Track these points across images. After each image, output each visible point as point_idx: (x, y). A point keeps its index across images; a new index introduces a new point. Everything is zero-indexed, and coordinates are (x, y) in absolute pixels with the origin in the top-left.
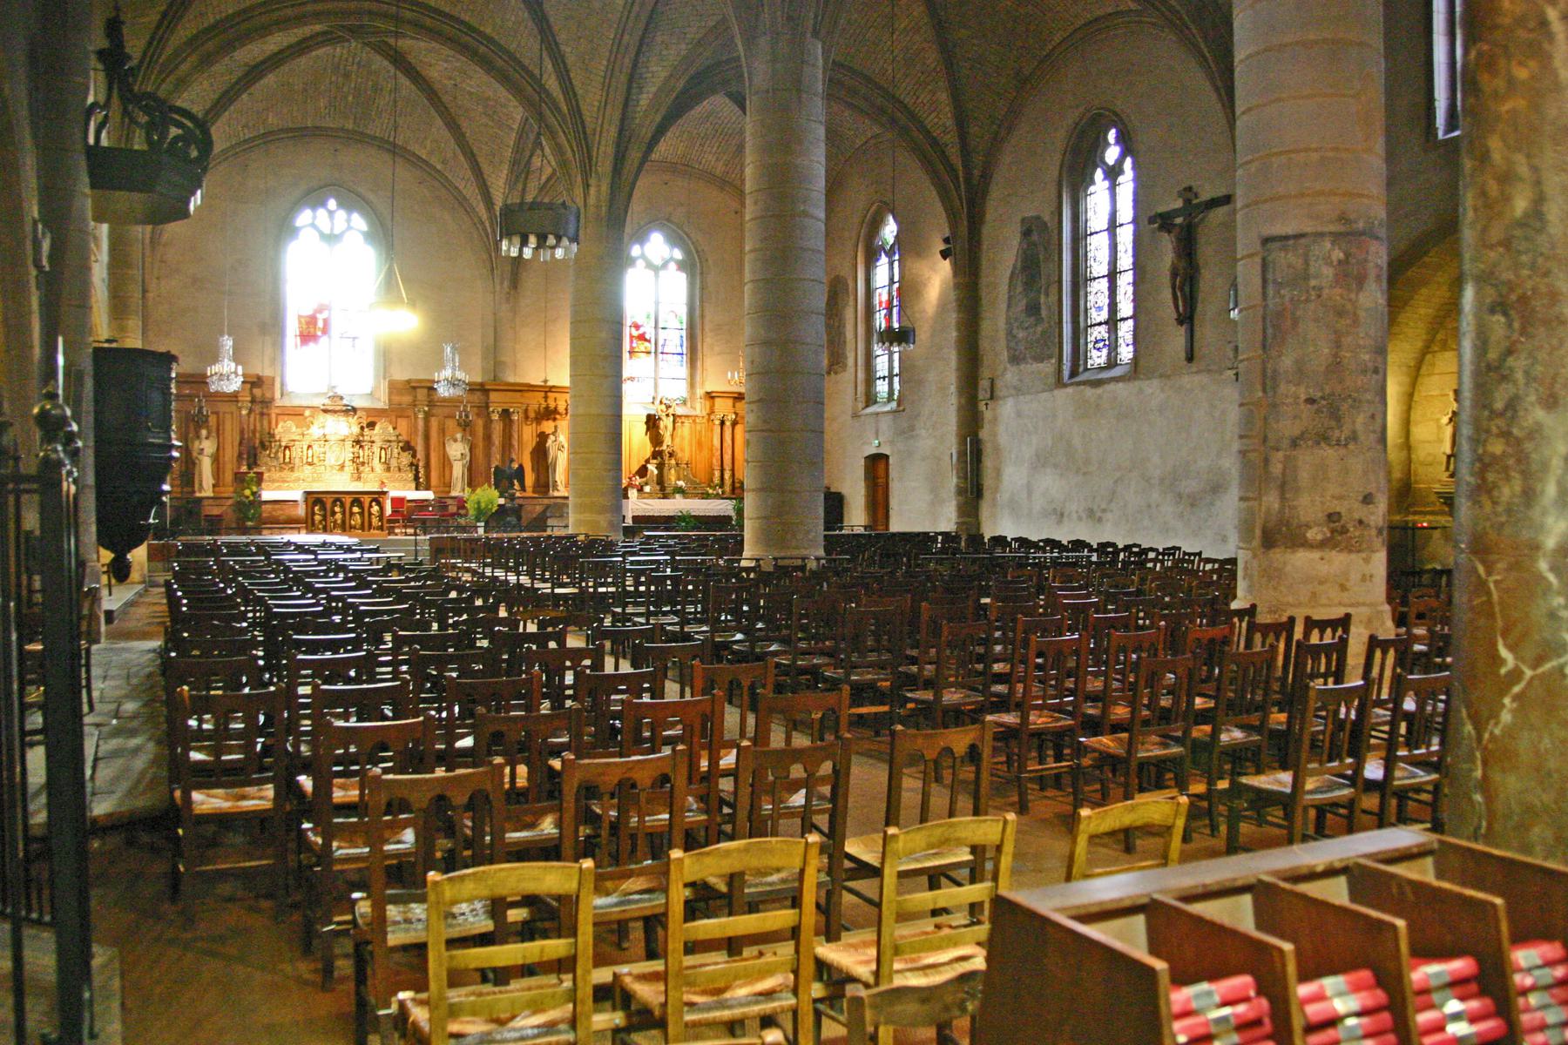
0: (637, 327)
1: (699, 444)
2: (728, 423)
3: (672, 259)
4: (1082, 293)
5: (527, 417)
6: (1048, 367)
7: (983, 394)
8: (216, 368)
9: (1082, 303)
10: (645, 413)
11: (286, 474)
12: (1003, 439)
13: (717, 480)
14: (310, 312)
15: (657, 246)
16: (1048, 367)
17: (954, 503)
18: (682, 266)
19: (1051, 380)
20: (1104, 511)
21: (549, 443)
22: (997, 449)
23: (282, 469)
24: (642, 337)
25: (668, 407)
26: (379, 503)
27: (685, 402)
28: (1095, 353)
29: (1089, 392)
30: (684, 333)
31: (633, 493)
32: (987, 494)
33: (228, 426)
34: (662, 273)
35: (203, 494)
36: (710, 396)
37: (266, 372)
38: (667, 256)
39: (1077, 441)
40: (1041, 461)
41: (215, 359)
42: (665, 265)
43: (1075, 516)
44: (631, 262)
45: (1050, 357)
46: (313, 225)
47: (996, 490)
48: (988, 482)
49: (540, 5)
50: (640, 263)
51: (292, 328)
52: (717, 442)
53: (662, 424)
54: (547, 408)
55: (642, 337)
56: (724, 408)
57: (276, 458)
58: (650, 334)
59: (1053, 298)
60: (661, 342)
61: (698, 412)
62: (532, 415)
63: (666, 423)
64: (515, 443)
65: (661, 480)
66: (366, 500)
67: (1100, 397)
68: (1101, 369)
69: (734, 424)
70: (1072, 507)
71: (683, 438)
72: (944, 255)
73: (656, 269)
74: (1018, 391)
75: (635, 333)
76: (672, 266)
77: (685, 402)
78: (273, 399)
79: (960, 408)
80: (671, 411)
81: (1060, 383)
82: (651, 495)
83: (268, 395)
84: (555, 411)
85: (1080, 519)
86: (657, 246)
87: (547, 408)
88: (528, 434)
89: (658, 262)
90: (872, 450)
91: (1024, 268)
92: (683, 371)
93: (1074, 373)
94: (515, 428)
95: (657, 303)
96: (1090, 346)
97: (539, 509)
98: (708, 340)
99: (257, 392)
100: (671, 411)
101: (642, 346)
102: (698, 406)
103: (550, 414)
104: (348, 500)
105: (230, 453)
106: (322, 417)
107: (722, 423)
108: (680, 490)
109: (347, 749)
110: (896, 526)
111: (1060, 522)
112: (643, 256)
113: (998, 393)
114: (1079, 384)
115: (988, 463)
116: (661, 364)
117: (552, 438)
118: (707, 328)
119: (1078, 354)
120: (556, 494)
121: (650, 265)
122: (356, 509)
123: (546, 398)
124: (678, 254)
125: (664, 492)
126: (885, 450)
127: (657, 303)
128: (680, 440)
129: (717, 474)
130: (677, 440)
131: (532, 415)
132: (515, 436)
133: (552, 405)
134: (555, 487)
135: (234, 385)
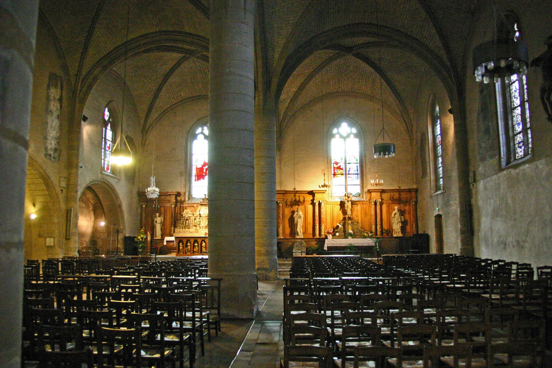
0: (337, 163)
1: (366, 214)
2: (378, 204)
3: (351, 133)
4: (510, 118)
5: (286, 205)
6: (494, 161)
7: (471, 180)
8: (149, 189)
9: (510, 122)
10: (339, 200)
11: (187, 230)
12: (480, 203)
13: (374, 230)
14: (200, 166)
15: (345, 128)
16: (494, 161)
17: (460, 238)
18: (356, 136)
19: (497, 168)
20: (524, 242)
21: (295, 215)
22: (478, 208)
23: (185, 228)
24: (339, 168)
25: (348, 197)
26: (205, 242)
27: (360, 195)
28: (519, 150)
29: (513, 171)
30: (358, 165)
31: (330, 237)
32: (476, 233)
33: (168, 211)
34: (347, 139)
35: (157, 238)
36: (370, 192)
37: (182, 191)
38: (349, 132)
39: (509, 201)
40: (496, 213)
41: (149, 186)
42: (348, 136)
43: (511, 246)
44: (333, 136)
45: (495, 155)
46: (202, 133)
47: (479, 231)
48: (476, 227)
49: (200, 2)
50: (337, 136)
51: (194, 172)
52: (373, 212)
53: (346, 205)
54: (295, 200)
55: (339, 168)
56: (376, 196)
57: (183, 223)
58: (343, 166)
59: (495, 122)
60: (348, 169)
61: (364, 199)
62: (289, 203)
63: (348, 205)
64: (281, 216)
65: (345, 231)
66: (199, 241)
67: (518, 174)
68: (522, 158)
69: (381, 204)
70: (510, 239)
71: (357, 211)
72: (450, 111)
73: (344, 138)
74: (485, 176)
75: (336, 166)
76: (352, 136)
77: (360, 195)
78: (185, 201)
79: (460, 189)
80: (349, 199)
81: (501, 170)
82: (339, 237)
83: (183, 199)
84: (299, 201)
85: (514, 246)
86: (345, 128)
87: (295, 200)
88: (287, 211)
89: (345, 135)
90: (436, 213)
91: (482, 110)
92: (358, 182)
93: (508, 162)
94: (281, 209)
95: (345, 152)
96: (517, 146)
97: (290, 243)
98: (368, 167)
99: (179, 198)
100: (349, 199)
101: (339, 172)
102: (364, 196)
103: (297, 203)
104: (192, 241)
105: (168, 222)
106: (200, 207)
107: (375, 204)
108: (350, 235)
109: (162, 354)
110: (446, 252)
111: (505, 248)
112: (338, 133)
113: (477, 179)
114: (511, 167)
115: (475, 215)
116: (348, 179)
117: (296, 213)
118: (367, 162)
119: (510, 151)
120: (298, 237)
121: (341, 137)
122: (196, 244)
123: (295, 196)
124: (354, 130)
125: (346, 235)
126: (441, 213)
127: (345, 152)
128: (358, 213)
129: (373, 227)
130: (355, 212)
131: (289, 203)
132: (281, 213)
133: (297, 199)
134: (298, 235)
135: (155, 196)
